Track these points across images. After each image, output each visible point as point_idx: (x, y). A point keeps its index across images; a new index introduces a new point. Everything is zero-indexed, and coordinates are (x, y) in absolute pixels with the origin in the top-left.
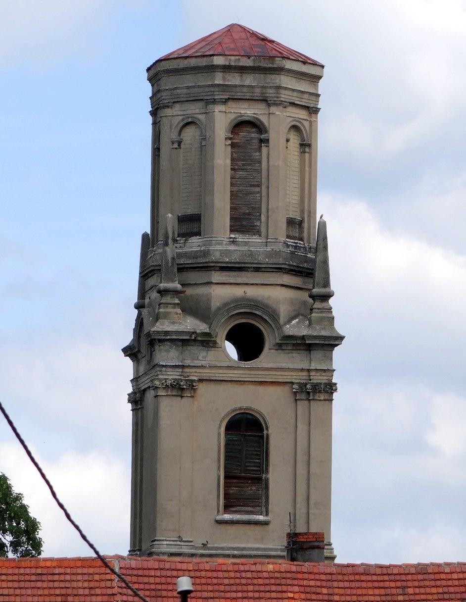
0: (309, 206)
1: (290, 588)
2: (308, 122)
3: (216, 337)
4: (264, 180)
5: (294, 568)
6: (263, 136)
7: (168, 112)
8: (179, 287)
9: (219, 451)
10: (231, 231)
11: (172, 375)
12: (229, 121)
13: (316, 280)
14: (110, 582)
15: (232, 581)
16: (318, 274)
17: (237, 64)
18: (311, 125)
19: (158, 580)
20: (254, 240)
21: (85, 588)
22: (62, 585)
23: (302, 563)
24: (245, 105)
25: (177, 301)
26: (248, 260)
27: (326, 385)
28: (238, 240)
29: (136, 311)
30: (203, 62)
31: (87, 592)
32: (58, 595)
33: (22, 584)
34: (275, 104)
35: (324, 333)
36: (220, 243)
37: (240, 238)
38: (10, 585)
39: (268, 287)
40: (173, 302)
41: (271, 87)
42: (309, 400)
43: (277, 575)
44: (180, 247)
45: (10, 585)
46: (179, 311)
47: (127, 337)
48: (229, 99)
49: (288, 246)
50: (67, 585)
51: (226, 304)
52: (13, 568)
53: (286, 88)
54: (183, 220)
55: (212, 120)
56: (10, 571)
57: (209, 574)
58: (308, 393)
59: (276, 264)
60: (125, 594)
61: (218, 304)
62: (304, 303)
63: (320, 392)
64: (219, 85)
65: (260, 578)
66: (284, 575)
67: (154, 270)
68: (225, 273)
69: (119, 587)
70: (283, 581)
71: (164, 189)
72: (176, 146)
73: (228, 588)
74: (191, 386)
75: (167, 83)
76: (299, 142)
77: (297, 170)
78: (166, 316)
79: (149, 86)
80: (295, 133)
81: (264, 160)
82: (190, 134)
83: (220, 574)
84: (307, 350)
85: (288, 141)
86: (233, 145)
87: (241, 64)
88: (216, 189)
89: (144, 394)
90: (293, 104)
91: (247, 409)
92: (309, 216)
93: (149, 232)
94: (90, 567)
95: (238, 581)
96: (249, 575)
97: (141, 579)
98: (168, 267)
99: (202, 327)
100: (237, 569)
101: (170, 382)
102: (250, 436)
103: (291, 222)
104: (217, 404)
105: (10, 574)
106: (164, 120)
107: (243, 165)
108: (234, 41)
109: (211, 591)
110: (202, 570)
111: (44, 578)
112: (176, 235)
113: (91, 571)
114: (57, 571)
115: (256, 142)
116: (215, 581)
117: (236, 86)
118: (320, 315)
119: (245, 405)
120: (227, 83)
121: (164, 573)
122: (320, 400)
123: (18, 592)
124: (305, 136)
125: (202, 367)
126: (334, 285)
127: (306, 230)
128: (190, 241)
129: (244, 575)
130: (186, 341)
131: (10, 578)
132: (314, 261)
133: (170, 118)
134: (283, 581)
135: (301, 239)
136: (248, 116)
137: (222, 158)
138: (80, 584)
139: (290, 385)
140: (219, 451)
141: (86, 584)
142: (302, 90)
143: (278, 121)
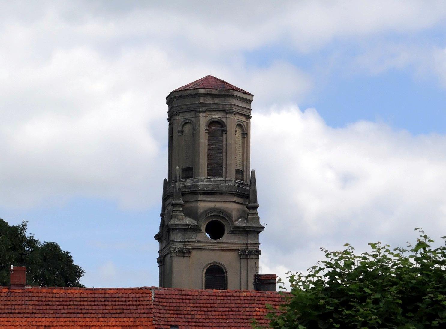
0: (247, 164)
1: (257, 306)
2: (246, 123)
3: (201, 227)
4: (224, 150)
5: (259, 294)
6: (224, 129)
7: (177, 117)
8: (182, 202)
9: (202, 284)
10: (208, 175)
11: (179, 246)
12: (207, 121)
13: (250, 199)
14: (149, 302)
15: (222, 302)
16: (251, 197)
17: (211, 93)
18: (247, 124)
19: (178, 301)
20: (219, 180)
21: (134, 305)
22: (120, 303)
23: (263, 292)
24: (215, 113)
25: (181, 209)
26: (216, 189)
27: (256, 251)
28: (211, 179)
29: (157, 244)
30: (194, 92)
31: (135, 307)
32: (118, 309)
33: (96, 303)
34: (230, 113)
35: (254, 225)
36: (203, 181)
37: (213, 179)
38: (89, 303)
39: (227, 202)
40: (179, 210)
41: (228, 104)
42: (247, 259)
43: (249, 298)
44: (183, 183)
45: (89, 303)
46: (182, 214)
47: (157, 230)
48: (207, 110)
49: (236, 183)
50: (124, 303)
51: (206, 211)
52: (91, 294)
53: (235, 105)
54: (184, 170)
55: (199, 121)
56: (89, 296)
57: (208, 298)
58: (247, 255)
59: (231, 191)
60: (158, 309)
61: (202, 211)
62: (244, 211)
63: (253, 254)
64: (202, 103)
65: (239, 300)
66: (253, 298)
67: (169, 195)
68: (205, 196)
69: (155, 305)
70: (253, 302)
71: (175, 143)
72: (181, 134)
73: (219, 305)
74: (189, 251)
75: (176, 103)
76: (241, 132)
77: (241, 146)
78: (176, 216)
79: (156, 245)
80: (239, 128)
81: (224, 140)
82: (187, 128)
83: (215, 298)
84: (246, 234)
85: (236, 131)
86: (209, 133)
87: (213, 93)
88: (200, 155)
89: (165, 258)
90: (238, 113)
91: (216, 263)
92: (247, 169)
93: (167, 179)
94: (137, 293)
95: (225, 301)
96: (232, 298)
97: (167, 301)
98: (178, 192)
99: (194, 222)
100: (225, 295)
101: (178, 249)
102: (218, 276)
103: (237, 171)
104: (202, 260)
105: (89, 297)
106: (175, 121)
107: (214, 143)
108: (209, 82)
109: (210, 307)
110: (204, 296)
111: (110, 299)
112: (181, 178)
113: (138, 295)
114: (117, 295)
115: (220, 131)
116: (212, 302)
117: (210, 104)
118: (252, 216)
119: (215, 261)
120: (206, 102)
121: (181, 297)
122: (253, 259)
123: (94, 307)
124: (244, 129)
125: (194, 242)
126: (259, 202)
127: (245, 176)
128: (188, 180)
129: (229, 298)
130: (185, 229)
131: (89, 299)
132: (249, 191)
133: (178, 120)
134: (253, 302)
135: (243, 180)
136: (216, 119)
137: (203, 139)
138: (131, 303)
139: (238, 251)
140: (202, 284)
141: (134, 303)
142: (243, 106)
143: (231, 121)
